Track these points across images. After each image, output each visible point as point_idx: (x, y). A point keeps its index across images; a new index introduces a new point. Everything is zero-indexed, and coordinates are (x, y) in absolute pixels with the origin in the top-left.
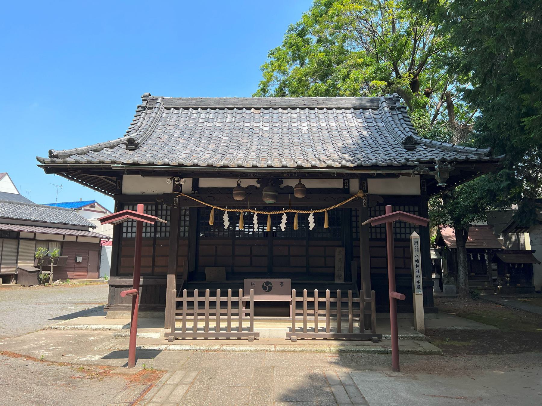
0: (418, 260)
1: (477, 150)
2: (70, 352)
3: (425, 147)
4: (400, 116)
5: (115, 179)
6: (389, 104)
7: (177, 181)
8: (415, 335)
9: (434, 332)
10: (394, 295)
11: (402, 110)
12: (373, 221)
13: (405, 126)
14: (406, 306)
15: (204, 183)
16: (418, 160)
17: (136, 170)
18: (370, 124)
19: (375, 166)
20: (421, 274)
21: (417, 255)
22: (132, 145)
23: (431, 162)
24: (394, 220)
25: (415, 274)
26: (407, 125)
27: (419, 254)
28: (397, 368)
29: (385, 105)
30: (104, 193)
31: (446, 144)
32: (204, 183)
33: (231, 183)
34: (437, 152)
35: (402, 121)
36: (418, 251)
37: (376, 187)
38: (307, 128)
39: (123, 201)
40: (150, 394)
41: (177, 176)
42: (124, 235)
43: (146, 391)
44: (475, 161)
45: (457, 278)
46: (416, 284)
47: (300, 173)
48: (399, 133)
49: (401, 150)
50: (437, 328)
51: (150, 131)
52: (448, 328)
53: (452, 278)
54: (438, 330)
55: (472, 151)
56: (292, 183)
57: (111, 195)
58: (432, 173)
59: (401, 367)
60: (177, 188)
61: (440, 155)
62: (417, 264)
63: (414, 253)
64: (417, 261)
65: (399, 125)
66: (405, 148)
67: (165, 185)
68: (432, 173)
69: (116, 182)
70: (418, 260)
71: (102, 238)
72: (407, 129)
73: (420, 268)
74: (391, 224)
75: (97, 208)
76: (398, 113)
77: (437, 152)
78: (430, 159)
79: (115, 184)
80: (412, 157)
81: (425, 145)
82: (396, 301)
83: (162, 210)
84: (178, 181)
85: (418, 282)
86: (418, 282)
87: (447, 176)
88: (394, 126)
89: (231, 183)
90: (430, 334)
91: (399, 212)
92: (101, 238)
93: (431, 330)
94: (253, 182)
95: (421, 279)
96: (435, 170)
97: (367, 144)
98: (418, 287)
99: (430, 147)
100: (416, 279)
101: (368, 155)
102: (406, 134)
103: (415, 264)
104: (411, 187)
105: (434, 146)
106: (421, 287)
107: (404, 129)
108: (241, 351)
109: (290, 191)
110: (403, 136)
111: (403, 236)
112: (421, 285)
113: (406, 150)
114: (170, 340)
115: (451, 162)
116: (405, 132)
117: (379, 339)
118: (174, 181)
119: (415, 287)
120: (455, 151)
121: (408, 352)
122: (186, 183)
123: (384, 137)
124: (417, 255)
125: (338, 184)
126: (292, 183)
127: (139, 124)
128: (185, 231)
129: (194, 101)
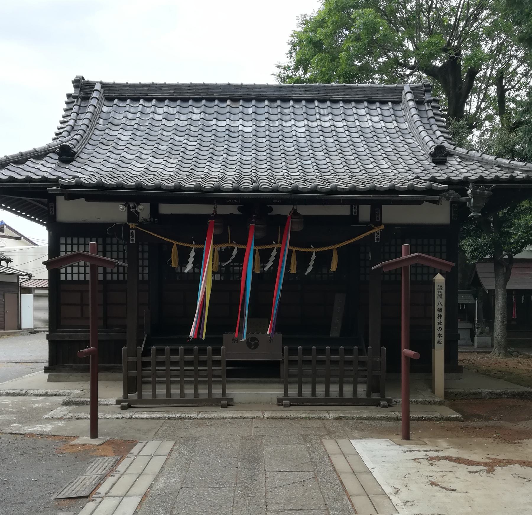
0: (441, 309)
1: (525, 165)
2: (14, 422)
3: (459, 160)
4: (430, 114)
5: (45, 200)
6: (415, 95)
7: (133, 208)
8: (431, 399)
9: (456, 395)
10: (407, 352)
11: (433, 104)
12: (385, 266)
13: (435, 127)
14: (423, 366)
15: (165, 209)
16: (448, 181)
17: (79, 191)
18: (389, 125)
19: (392, 190)
20: (443, 327)
21: (440, 303)
22: (66, 154)
23: (466, 181)
24: (413, 262)
25: (437, 326)
26: (439, 126)
27: (443, 301)
28: (407, 437)
29: (409, 96)
30: (30, 218)
31: (486, 157)
32: (165, 209)
33: (205, 209)
34: (475, 167)
35: (433, 121)
36: (441, 298)
37: (392, 215)
38: (303, 130)
39: (59, 232)
40: (121, 468)
41: (132, 201)
42: (63, 277)
43: (117, 463)
44: (522, 181)
45: (492, 328)
46: (437, 338)
47: (296, 197)
48: (427, 139)
49: (428, 163)
50: (460, 390)
51: (89, 134)
52: (472, 391)
53: (487, 328)
54: (460, 393)
55: (520, 166)
56: (285, 210)
57: (42, 224)
58: (463, 199)
59: (412, 435)
60: (133, 216)
61: (478, 171)
62: (440, 313)
63: (437, 301)
64: (440, 310)
65: (428, 127)
66: (433, 162)
67: (116, 213)
68: (463, 199)
69: (47, 205)
70: (441, 309)
71: (21, 275)
72: (438, 133)
73: (443, 319)
74: (406, 268)
75: (7, 232)
76: (427, 108)
77: (475, 167)
78: (464, 177)
79: (46, 208)
80: (441, 174)
81: (460, 157)
82: (411, 360)
83: (112, 244)
84: (135, 207)
85: (440, 335)
86: (440, 335)
87: (482, 204)
88: (421, 128)
89: (205, 209)
90: (451, 398)
91: (417, 254)
92: (18, 275)
93: (453, 393)
94: (232, 209)
95: (443, 333)
96: (467, 195)
97: (384, 155)
98: (439, 342)
99: (467, 160)
100: (437, 333)
101: (385, 171)
102: (436, 140)
103: (437, 313)
104: (439, 215)
105: (471, 159)
106: (443, 342)
107: (434, 133)
108: (223, 418)
109: (282, 220)
110: (431, 144)
111: (425, 278)
112: (443, 339)
113: (434, 165)
114: (123, 408)
115: (492, 181)
116: (434, 137)
117: (390, 404)
118: (129, 208)
119: (436, 342)
120: (498, 166)
121: (420, 419)
122: (144, 210)
123: (407, 143)
124: (440, 303)
125: (344, 210)
126: (285, 210)
127: (71, 122)
128: (145, 274)
129: (146, 89)
